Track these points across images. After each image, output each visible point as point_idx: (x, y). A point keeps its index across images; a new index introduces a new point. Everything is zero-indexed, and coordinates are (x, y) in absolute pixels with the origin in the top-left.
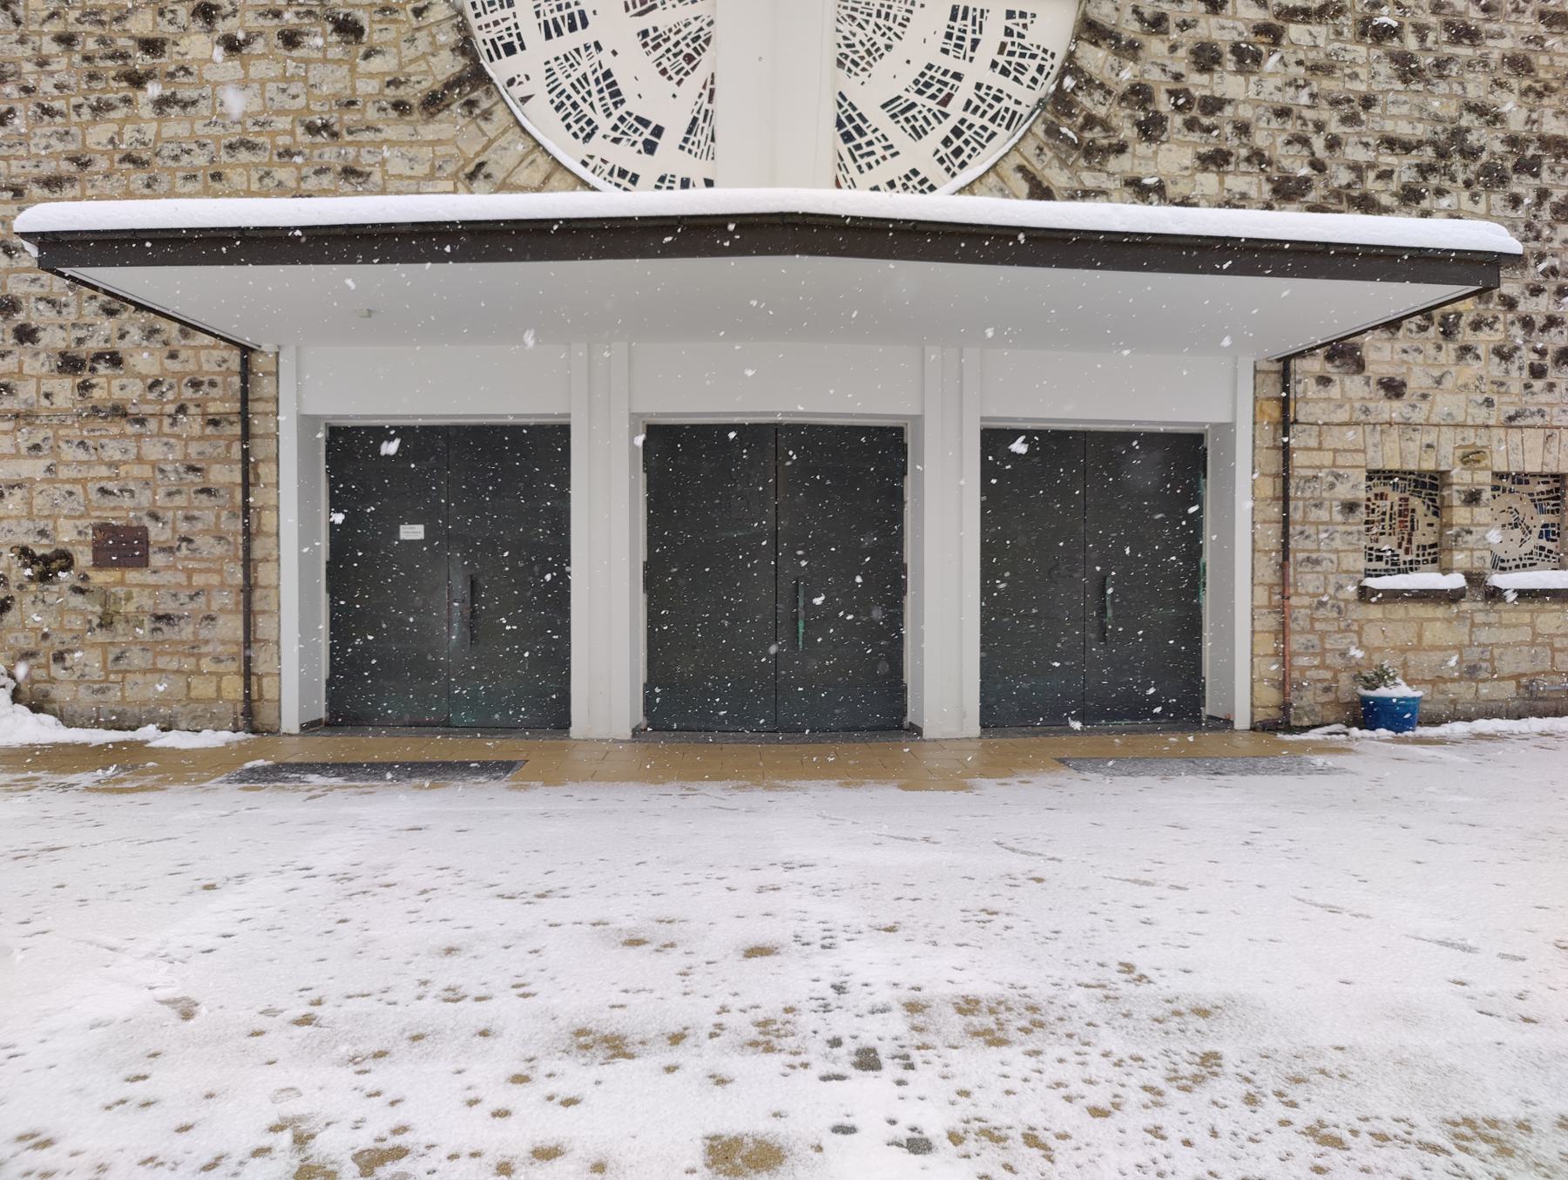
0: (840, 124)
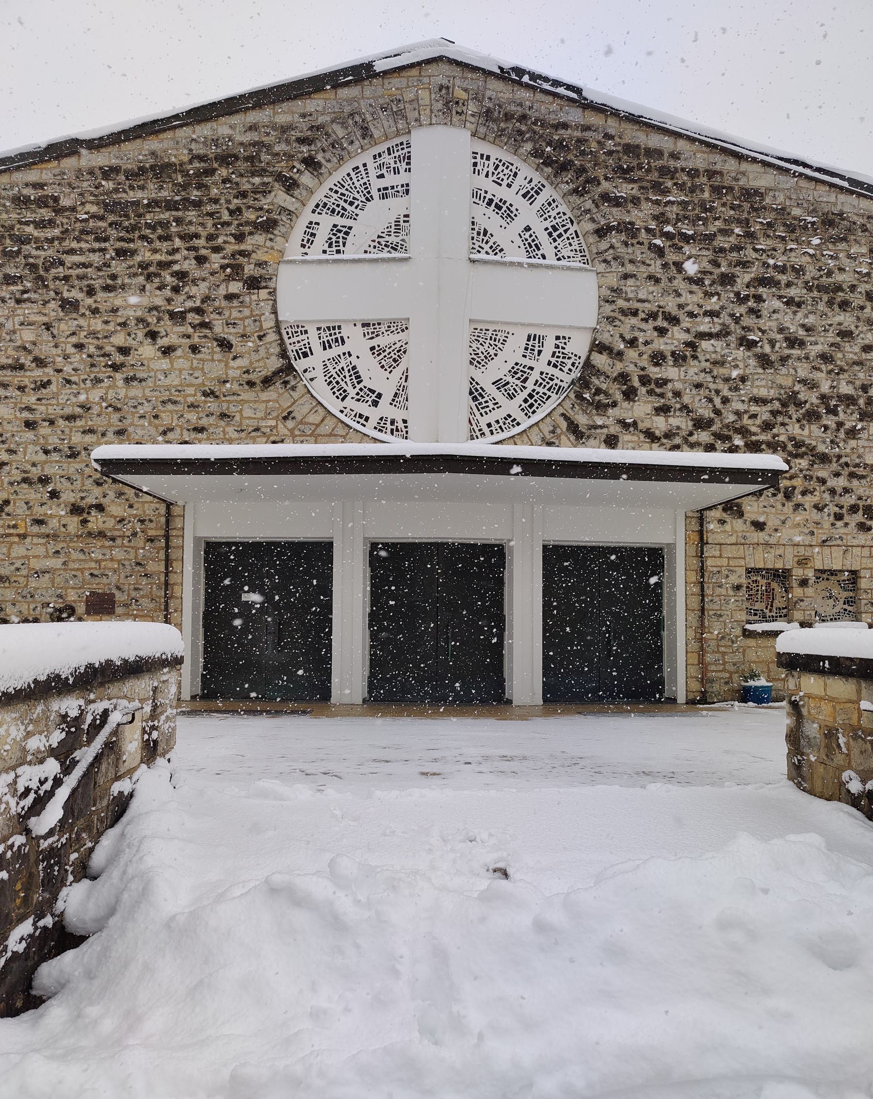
0: (471, 393)
